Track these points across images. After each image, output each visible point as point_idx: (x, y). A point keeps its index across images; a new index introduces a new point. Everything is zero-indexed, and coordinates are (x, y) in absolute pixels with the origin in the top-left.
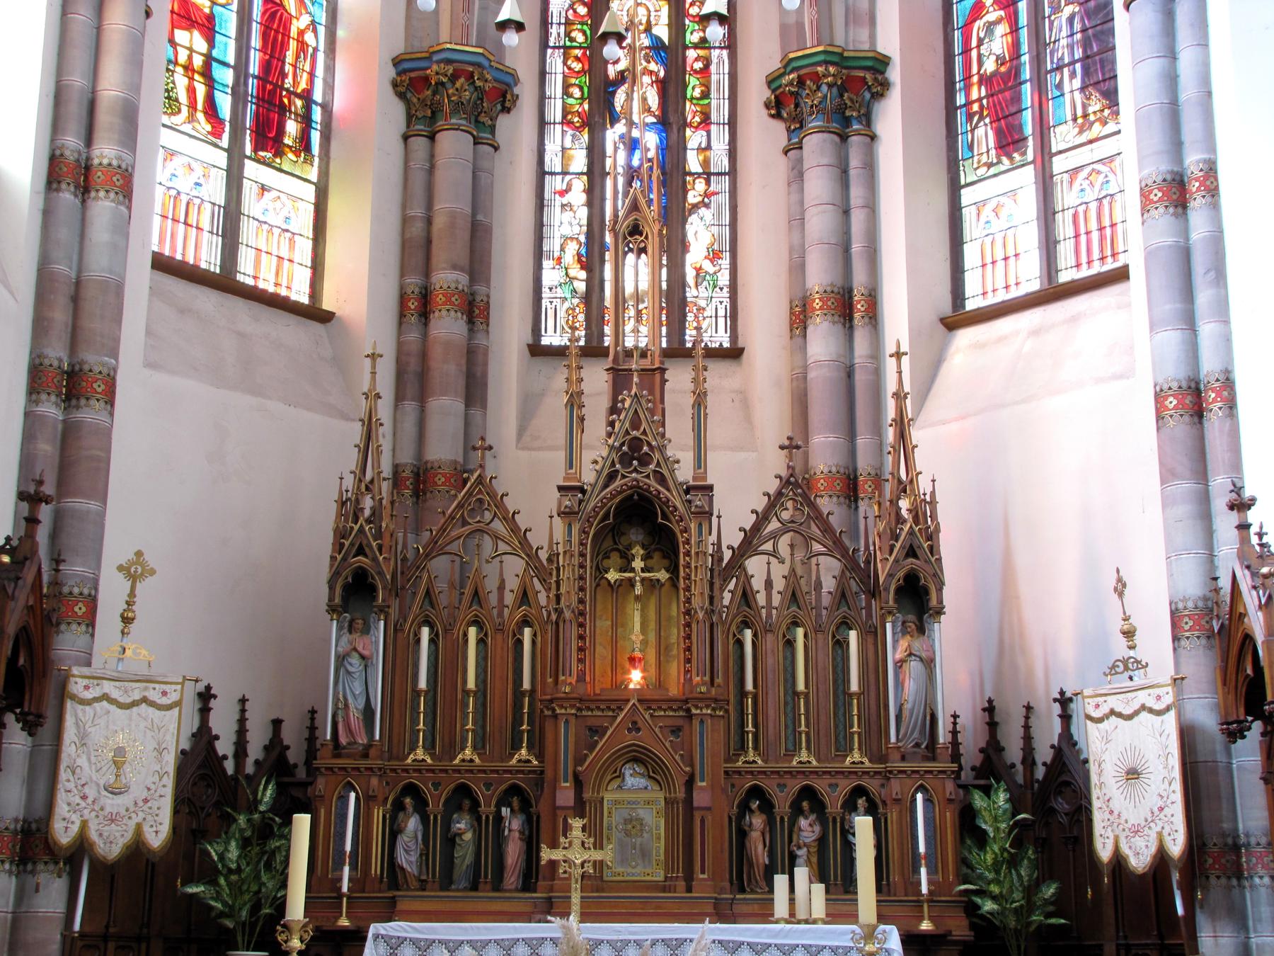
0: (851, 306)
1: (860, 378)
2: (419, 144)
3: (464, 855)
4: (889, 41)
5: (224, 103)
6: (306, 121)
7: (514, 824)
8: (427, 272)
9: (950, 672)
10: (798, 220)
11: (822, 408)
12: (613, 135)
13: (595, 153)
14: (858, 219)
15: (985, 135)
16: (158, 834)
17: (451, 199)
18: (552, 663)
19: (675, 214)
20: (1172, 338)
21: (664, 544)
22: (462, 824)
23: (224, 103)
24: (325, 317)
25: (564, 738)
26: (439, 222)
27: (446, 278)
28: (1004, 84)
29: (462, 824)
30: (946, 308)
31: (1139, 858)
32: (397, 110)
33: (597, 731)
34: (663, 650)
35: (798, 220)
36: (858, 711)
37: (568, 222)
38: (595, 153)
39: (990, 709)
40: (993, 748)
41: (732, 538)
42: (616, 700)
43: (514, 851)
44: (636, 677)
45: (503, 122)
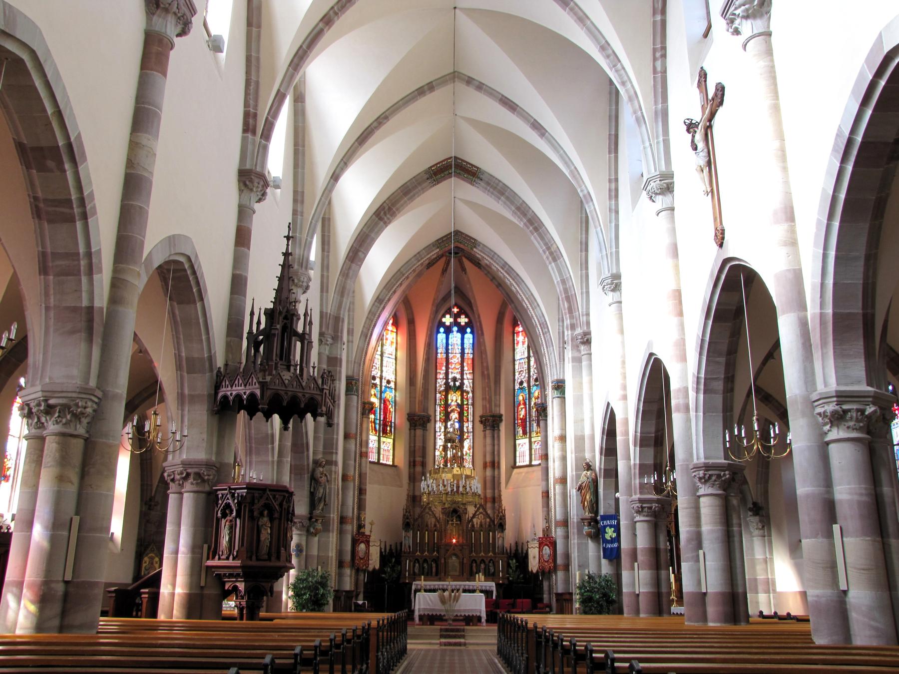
0: (494, 465)
1: (496, 479)
2: (412, 431)
3: (426, 570)
4: (503, 412)
5: (377, 427)
6: (391, 426)
7: (434, 565)
8: (414, 457)
9: (508, 537)
10: (485, 446)
11: (489, 485)
12: (449, 423)
13: (446, 427)
14: (496, 447)
15: (520, 430)
16: (377, 567)
17: (419, 444)
18: (440, 538)
19: (462, 440)
20: (544, 483)
21: (459, 518)
22: (425, 565)
23: (377, 427)
24: (396, 466)
25: (442, 551)
26: (417, 448)
27: (418, 459)
28: (524, 420)
29: (425, 565)
30: (512, 463)
31: (535, 571)
32: (408, 424)
33: (448, 550)
34: (459, 535)
35: (485, 446)
36: (490, 546)
37: (440, 442)
38: (446, 427)
39: (516, 543)
40: (517, 550)
41: (471, 515)
42: (451, 544)
43: (434, 570)
44: (454, 541)
45: (428, 425)
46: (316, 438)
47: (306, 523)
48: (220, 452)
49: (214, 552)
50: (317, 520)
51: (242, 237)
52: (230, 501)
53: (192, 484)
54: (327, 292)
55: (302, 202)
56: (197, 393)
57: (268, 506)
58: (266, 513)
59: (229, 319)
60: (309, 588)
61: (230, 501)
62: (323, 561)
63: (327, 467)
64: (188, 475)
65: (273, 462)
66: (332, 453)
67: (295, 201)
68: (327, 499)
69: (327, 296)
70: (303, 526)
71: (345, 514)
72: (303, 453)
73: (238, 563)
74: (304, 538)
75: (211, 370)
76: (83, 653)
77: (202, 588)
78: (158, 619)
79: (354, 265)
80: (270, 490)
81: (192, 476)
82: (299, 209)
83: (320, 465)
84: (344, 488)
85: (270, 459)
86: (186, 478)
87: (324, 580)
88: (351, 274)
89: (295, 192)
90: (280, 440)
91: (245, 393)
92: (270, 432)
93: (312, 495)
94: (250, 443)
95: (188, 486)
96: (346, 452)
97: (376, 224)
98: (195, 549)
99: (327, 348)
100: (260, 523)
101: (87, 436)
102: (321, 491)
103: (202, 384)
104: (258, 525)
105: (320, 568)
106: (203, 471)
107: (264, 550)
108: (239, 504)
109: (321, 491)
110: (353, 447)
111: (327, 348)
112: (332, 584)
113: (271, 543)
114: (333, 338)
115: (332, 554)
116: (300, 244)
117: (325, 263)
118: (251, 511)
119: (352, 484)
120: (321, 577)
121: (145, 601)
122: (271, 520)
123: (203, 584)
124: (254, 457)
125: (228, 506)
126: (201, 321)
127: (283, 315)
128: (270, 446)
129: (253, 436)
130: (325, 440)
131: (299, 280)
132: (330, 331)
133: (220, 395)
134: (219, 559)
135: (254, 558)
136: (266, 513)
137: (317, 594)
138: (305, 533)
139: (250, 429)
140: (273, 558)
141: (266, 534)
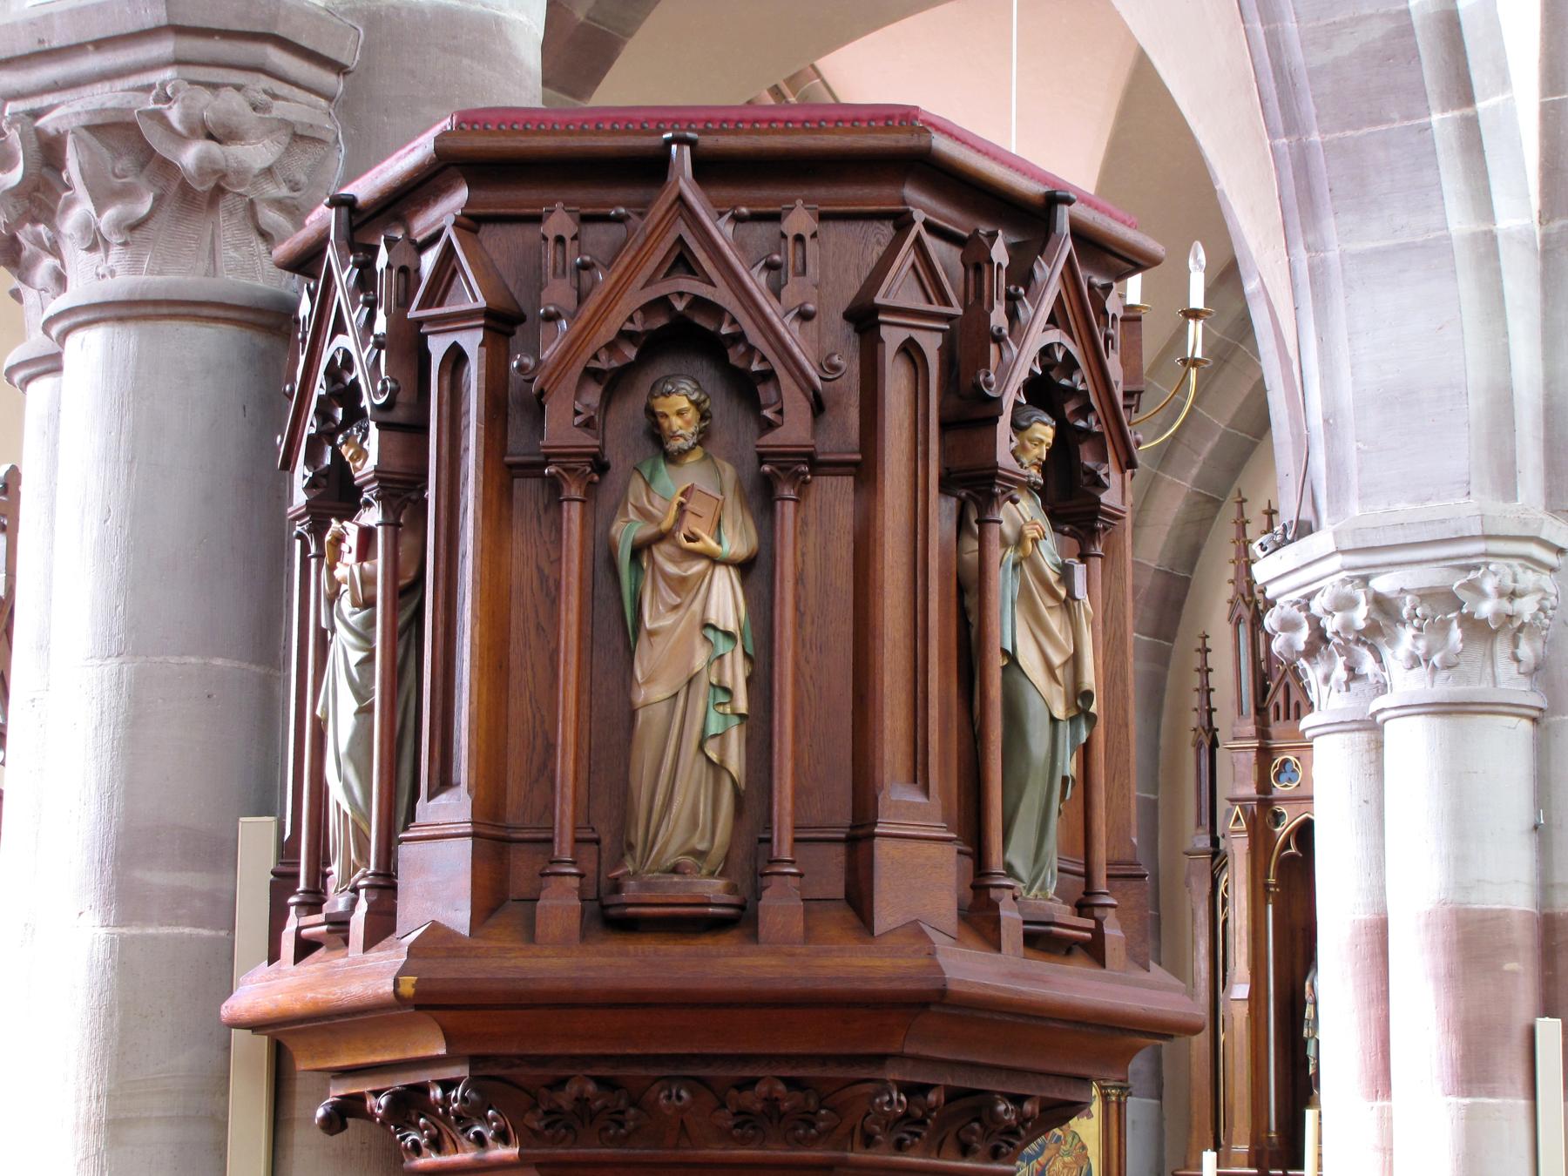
53: (96, 243)
57: (685, 335)
58: (679, 408)
64: (50, 152)
65: (1488, 246)
80: (710, 168)
85: (1458, 221)
86: (1373, 636)
95: (1402, 673)
101: (1537, 700)
106: (159, 89)
107: (685, 819)
113: (759, 728)
129: (1298, 57)
135: (561, 903)
136: (679, 408)
140: (780, 907)
141: (696, 627)
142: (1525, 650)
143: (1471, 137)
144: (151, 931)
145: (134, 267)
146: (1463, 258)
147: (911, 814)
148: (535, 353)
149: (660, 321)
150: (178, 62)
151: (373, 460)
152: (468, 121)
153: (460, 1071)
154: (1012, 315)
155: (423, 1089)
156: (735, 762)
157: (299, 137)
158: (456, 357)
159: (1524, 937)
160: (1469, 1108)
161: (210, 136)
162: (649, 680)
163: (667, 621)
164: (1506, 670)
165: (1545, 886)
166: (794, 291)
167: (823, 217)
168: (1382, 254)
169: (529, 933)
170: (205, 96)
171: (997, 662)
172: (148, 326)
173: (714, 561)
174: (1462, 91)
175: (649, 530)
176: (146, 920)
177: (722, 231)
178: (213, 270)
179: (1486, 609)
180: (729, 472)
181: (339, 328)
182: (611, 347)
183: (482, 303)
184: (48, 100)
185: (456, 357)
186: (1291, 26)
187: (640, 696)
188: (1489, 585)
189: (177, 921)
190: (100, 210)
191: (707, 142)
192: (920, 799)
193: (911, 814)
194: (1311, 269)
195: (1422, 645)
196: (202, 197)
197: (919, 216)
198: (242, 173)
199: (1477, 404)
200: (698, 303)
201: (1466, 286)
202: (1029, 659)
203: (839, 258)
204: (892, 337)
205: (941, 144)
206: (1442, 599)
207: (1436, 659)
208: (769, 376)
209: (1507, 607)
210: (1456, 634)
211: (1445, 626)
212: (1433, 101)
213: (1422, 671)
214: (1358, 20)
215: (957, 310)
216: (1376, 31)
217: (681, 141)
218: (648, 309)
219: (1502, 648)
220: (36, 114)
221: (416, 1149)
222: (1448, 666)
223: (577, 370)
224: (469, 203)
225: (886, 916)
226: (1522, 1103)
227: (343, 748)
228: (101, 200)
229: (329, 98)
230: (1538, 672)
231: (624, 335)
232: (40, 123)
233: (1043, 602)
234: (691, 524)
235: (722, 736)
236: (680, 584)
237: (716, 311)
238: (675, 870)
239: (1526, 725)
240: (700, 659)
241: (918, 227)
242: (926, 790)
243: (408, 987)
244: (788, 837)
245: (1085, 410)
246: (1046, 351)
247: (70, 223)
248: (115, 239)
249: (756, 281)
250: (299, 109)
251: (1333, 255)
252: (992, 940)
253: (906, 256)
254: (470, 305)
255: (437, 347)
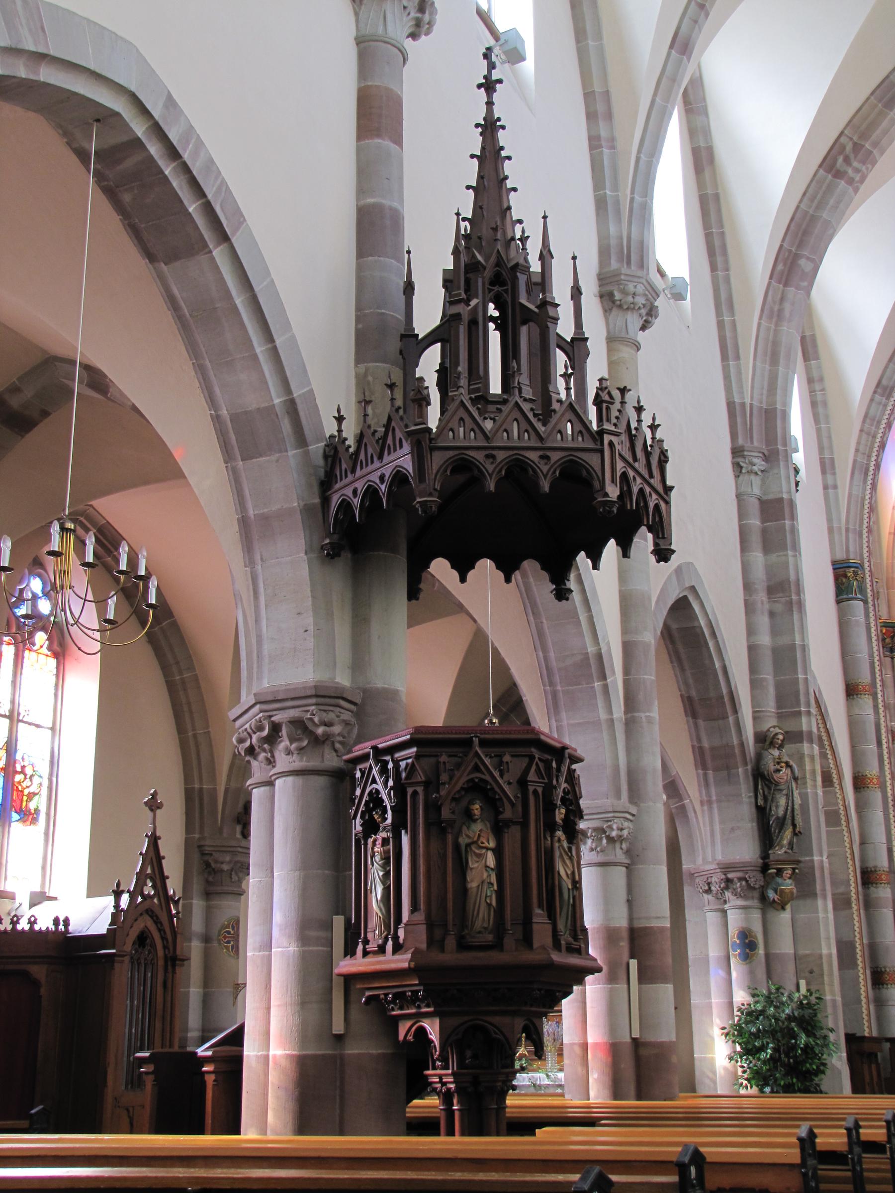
46: (755, 684)
47: (756, 879)
48: (359, 660)
49: (354, 937)
50: (780, 872)
51: (377, 116)
52: (379, 786)
53: (289, 752)
54: (737, 357)
55: (609, 116)
56: (275, 507)
57: (479, 789)
58: (476, 808)
59: (358, 320)
60: (773, 1033)
61: (379, 786)
62: (809, 968)
63: (789, 748)
64: (276, 728)
66: (799, 713)
67: (591, 116)
68: (799, 820)
69: (738, 368)
70: (750, 888)
71: (871, 864)
72: (725, 717)
73: (402, 961)
74: (756, 915)
75: (301, 440)
76: (791, 1113)
77: (339, 1038)
78: (249, 1135)
79: (791, 290)
80: (483, 743)
81: (284, 732)
82: (603, 133)
83: (772, 744)
84: (862, 807)
85: (603, 715)
86: (273, 738)
87: (807, 1012)
88: (787, 313)
89: (589, 96)
90: (627, 671)
91: (382, 478)
92: (591, 649)
93: (762, 813)
94: (551, 684)
96: (854, 725)
97: (830, 189)
98: (309, 929)
99: (756, 481)
100: (463, 841)
101: (627, 861)
102: (782, 801)
103: (284, 482)
104: (457, 847)
105: (803, 983)
106: (312, 713)
107: (482, 918)
108: (399, 790)
109: (782, 801)
110: (871, 711)
111: (756, 481)
112: (835, 1024)
113: (500, 893)
114: (766, 458)
115: (829, 949)
116: (618, 212)
117: (723, 296)
118: (433, 808)
119: (878, 795)
120: (801, 1005)
121: (210, 1079)
122: (498, 829)
123: (338, 1027)
124: (564, 715)
125: (375, 800)
126: (239, 301)
127: (488, 274)
128: (597, 685)
129: (554, 664)
130: (778, 686)
131: (624, 293)
132: (758, 442)
133: (335, 500)
134: (365, 953)
135: (451, 942)
136: (476, 808)
137: (794, 1047)
138: (755, 903)
139: (545, 650)
141: (482, 868)
142: (624, 846)
143: (606, 688)
144: (311, 948)
145: (301, 760)
146: (604, 726)
147: (539, 915)
148: (438, 792)
149: (470, 784)
150: (316, 704)
151: (389, 820)
152: (418, 730)
153: (422, 988)
154: (557, 781)
155: (404, 993)
156: (494, 903)
157: (347, 723)
158: (415, 793)
159: (625, 934)
160: (611, 988)
161: (326, 725)
162: (472, 881)
163: (476, 865)
164: (619, 852)
165: (631, 919)
166: (506, 777)
167: (512, 756)
168: (579, 724)
169: (443, 950)
170: (324, 714)
171: (557, 875)
172: (306, 777)
173: (487, 849)
174: (604, 677)
175: (469, 841)
176: (309, 945)
177: (487, 761)
178: (323, 761)
179: (614, 834)
180: (488, 825)
181: (374, 781)
182: (459, 792)
183: (423, 779)
184: (274, 713)
185: (415, 793)
186: (552, 654)
187: (469, 886)
188: (615, 827)
189: (318, 946)
190: (291, 744)
191: (482, 736)
192: (541, 912)
193: (539, 915)
194: (557, 727)
195: (594, 846)
196: (317, 742)
197: (537, 756)
198: (333, 735)
199: (609, 771)
200: (481, 780)
201: (605, 735)
202: (562, 873)
203: (516, 766)
204: (531, 789)
205: (542, 737)
206: (600, 831)
207: (598, 849)
208: (501, 799)
209: (620, 833)
210: (604, 841)
211: (601, 839)
212: (595, 679)
213: (594, 853)
214: (573, 655)
215: (546, 781)
216: (578, 658)
217: (476, 737)
218: (468, 781)
219: (618, 845)
220: (270, 717)
221: (393, 1009)
222: (602, 851)
223: (450, 798)
224: (417, 752)
225: (536, 944)
226: (626, 986)
227: (379, 898)
228: (292, 740)
229: (352, 712)
230: (628, 852)
231: (462, 788)
232: (273, 719)
233: (565, 857)
234: (482, 839)
235: (491, 896)
236: (479, 856)
237: (486, 782)
238: (480, 932)
239: (624, 869)
240: (485, 875)
241: (537, 759)
242: (543, 910)
243: (412, 965)
244: (509, 923)
245: (571, 804)
246: (564, 789)
247: (282, 746)
248: (296, 752)
249: (496, 774)
250: (347, 716)
251: (565, 723)
252: (560, 950)
253: (534, 767)
254: (420, 780)
255: (410, 791)
